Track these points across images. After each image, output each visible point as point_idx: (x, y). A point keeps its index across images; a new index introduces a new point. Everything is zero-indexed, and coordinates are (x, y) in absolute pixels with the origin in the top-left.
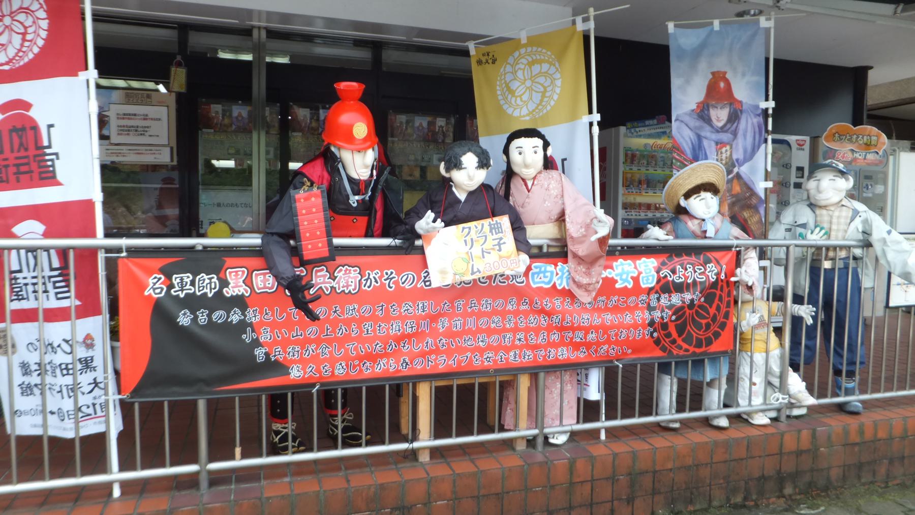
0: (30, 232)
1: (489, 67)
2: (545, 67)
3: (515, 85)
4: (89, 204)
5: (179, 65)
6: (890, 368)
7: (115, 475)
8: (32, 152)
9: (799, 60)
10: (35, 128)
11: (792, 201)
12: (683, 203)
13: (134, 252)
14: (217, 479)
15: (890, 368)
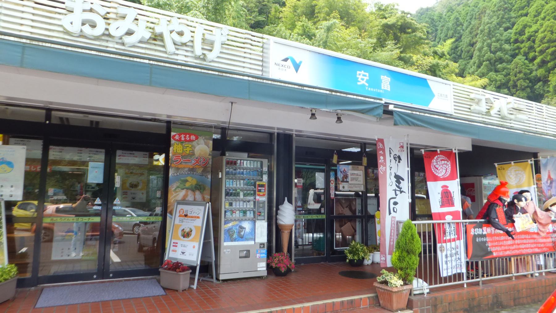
0: (449, 218)
1: (503, 171)
2: (520, 172)
3: (511, 176)
4: (459, 212)
5: (364, 156)
6: (503, 269)
7: (465, 281)
8: (449, 198)
9: (500, 148)
10: (450, 192)
11: (473, 195)
12: (550, 208)
13: (470, 223)
14: (484, 282)
15: (503, 269)
